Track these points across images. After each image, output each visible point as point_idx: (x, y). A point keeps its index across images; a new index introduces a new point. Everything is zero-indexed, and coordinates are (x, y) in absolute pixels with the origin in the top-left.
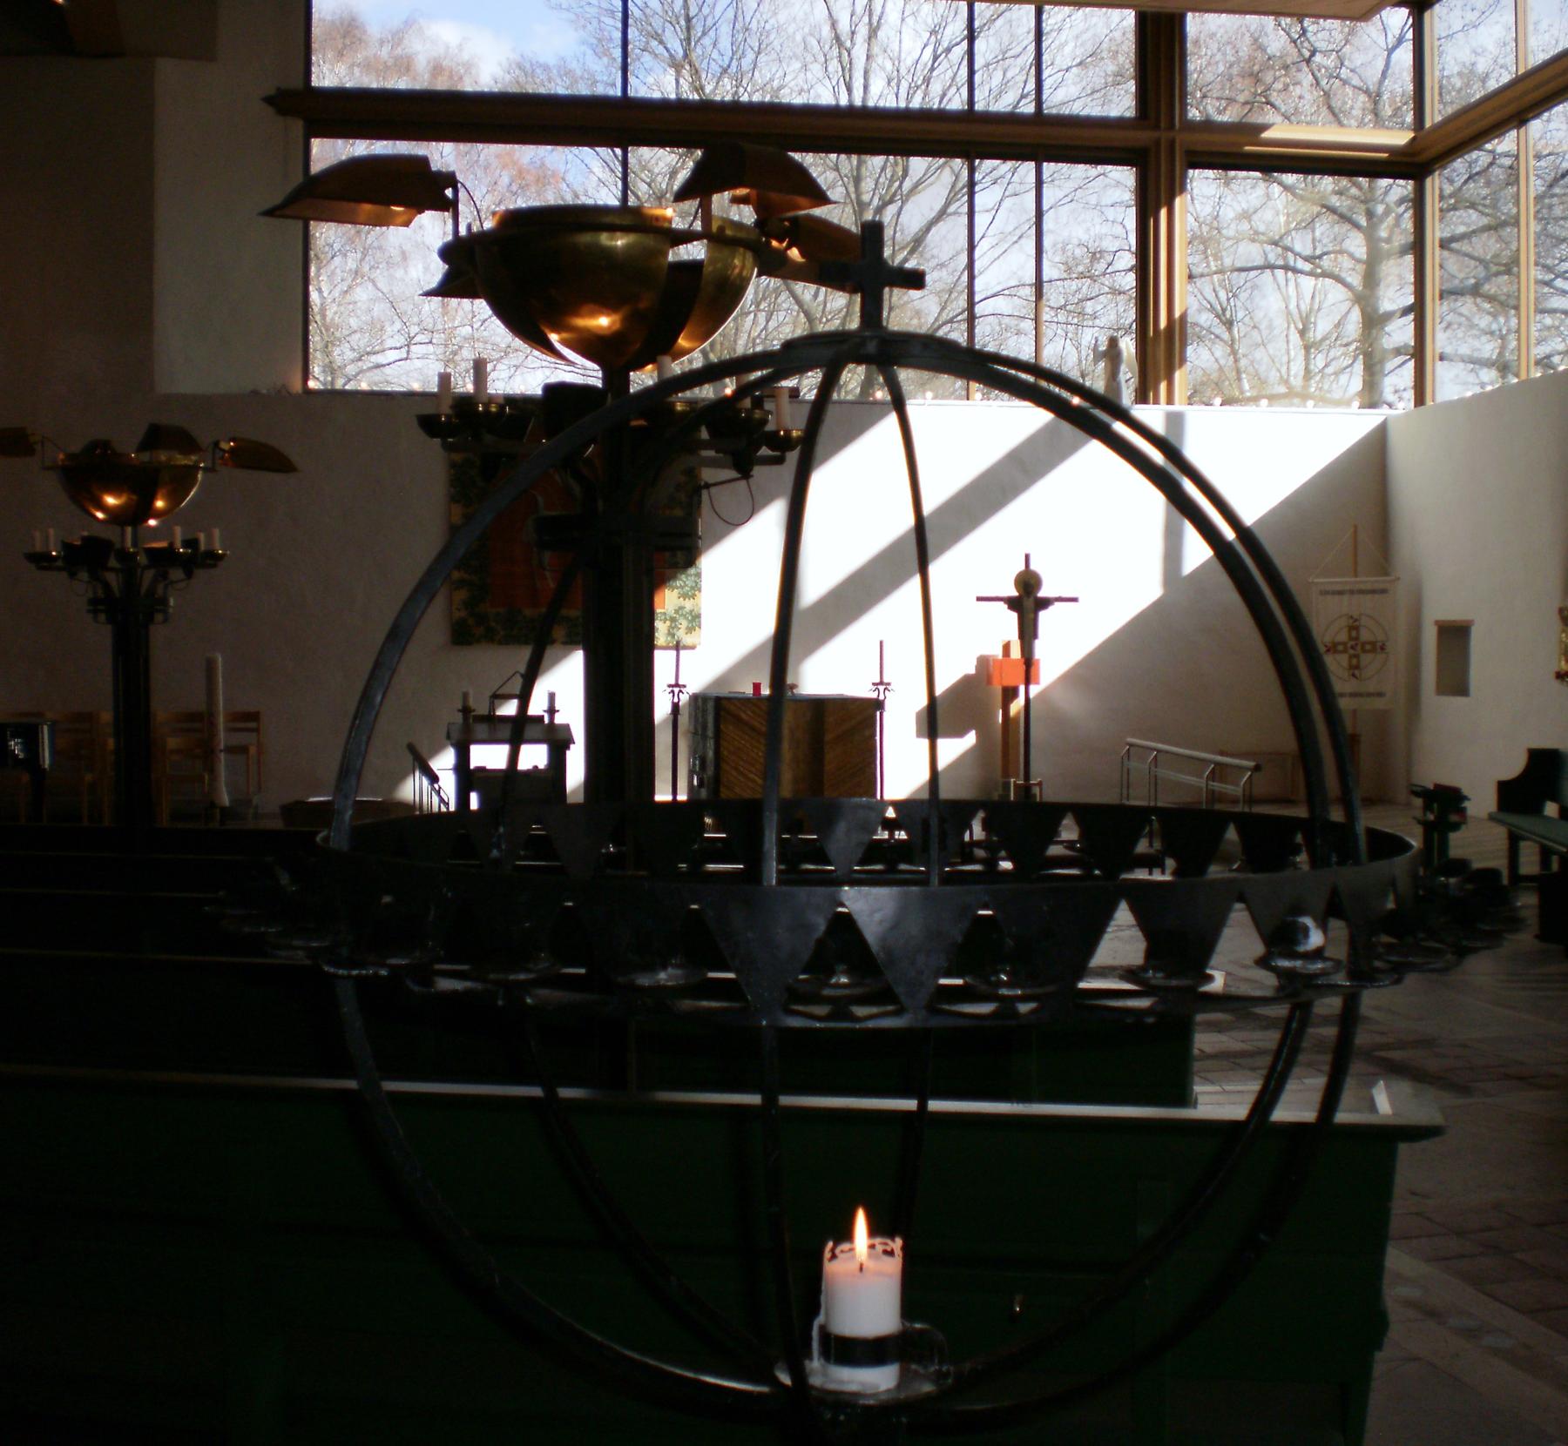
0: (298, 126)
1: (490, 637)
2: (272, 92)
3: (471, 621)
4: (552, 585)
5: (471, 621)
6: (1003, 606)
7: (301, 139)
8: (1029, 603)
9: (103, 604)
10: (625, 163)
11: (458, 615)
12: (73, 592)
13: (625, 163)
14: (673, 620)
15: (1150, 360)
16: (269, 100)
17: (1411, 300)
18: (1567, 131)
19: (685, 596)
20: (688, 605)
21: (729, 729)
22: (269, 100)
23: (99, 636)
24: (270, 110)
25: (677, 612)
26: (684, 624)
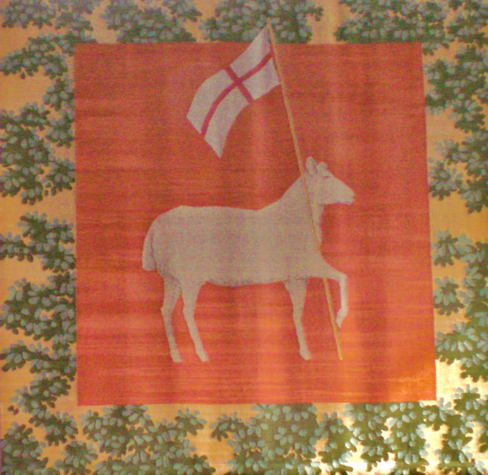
14: (453, 421)
25: (460, 404)
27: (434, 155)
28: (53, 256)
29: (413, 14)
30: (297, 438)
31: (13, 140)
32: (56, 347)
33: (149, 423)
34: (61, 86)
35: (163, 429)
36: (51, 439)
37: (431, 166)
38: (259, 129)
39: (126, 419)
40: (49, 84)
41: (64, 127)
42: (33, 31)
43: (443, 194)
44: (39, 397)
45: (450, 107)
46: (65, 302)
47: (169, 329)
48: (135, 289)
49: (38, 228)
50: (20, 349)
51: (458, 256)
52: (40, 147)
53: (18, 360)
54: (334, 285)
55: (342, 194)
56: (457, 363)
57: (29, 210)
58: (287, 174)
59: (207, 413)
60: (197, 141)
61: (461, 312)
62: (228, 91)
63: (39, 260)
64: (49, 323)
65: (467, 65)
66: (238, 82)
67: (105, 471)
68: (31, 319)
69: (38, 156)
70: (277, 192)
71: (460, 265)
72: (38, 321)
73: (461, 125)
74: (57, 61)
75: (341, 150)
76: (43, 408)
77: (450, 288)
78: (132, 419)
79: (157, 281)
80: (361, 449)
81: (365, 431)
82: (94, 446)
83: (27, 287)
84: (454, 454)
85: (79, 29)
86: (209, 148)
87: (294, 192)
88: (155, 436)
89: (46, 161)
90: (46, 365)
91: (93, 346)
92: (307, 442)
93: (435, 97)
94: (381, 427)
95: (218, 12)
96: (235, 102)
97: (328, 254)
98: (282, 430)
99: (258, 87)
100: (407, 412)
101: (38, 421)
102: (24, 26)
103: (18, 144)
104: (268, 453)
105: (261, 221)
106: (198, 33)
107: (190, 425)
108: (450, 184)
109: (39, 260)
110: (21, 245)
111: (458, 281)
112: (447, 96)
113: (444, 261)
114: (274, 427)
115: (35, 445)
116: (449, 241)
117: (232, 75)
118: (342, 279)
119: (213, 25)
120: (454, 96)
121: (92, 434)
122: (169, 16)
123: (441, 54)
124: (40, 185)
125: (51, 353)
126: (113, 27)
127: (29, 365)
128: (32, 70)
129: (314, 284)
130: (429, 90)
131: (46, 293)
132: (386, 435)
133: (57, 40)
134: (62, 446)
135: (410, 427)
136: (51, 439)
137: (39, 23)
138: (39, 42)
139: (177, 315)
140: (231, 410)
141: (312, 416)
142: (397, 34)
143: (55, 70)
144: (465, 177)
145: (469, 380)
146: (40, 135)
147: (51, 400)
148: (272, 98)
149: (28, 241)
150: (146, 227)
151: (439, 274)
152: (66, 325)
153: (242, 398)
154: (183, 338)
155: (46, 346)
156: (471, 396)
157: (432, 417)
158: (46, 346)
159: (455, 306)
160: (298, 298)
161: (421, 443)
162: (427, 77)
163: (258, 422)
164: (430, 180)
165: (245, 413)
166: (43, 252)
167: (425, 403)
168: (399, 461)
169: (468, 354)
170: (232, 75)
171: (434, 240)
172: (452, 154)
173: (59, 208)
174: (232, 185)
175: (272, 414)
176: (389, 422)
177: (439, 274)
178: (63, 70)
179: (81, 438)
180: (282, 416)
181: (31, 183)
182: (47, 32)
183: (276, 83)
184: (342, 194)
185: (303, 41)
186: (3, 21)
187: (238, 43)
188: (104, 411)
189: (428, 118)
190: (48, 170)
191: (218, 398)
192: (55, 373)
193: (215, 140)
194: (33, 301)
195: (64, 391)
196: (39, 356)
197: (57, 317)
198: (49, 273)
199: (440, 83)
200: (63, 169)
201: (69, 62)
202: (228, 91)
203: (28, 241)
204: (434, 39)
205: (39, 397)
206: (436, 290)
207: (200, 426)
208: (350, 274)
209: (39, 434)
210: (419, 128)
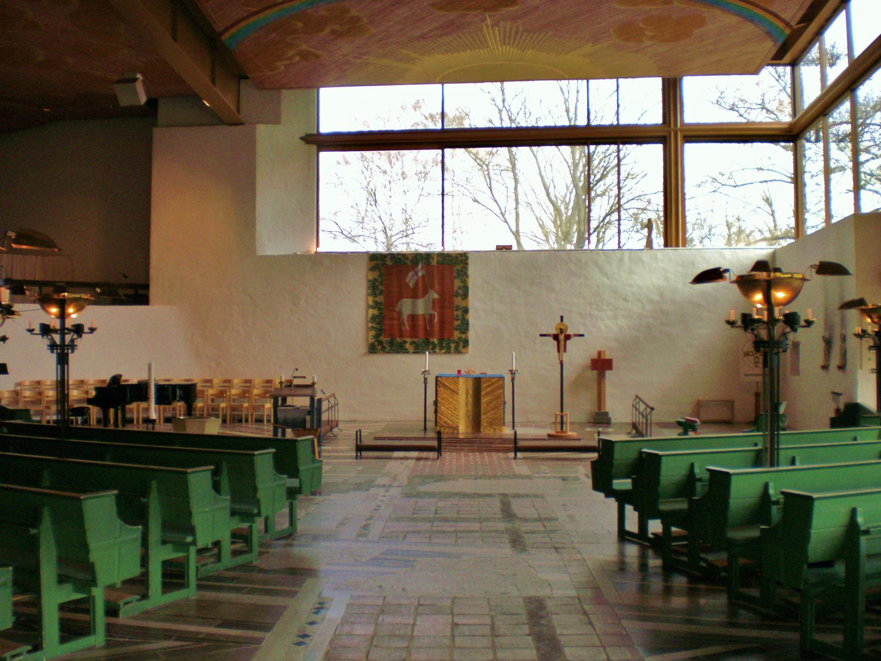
0: (315, 147)
1: (384, 350)
2: (304, 135)
3: (376, 344)
4: (408, 328)
5: (376, 344)
6: (551, 339)
7: (315, 152)
8: (562, 337)
9: (53, 346)
10: (618, 119)
11: (370, 341)
12: (43, 343)
13: (618, 119)
14: (457, 343)
15: (800, 205)
16: (302, 138)
17: (832, 176)
18: (880, 84)
19: (462, 333)
20: (463, 336)
21: (441, 390)
22: (302, 138)
23: (53, 358)
24: (302, 142)
26: (461, 344)
27: (455, 288)
28: (379, 309)
38: (420, 285)
47: (647, 614)
48: (395, 315)
55: (436, 296)
58: (425, 292)
59: (409, 340)
60: (407, 285)
66: (416, 273)
67: (378, 486)
75: (437, 287)
87: (427, 296)
91: (467, 42)
96: (415, 277)
99: (420, 274)
106: (409, 263)
107: (405, 342)
112: (459, 276)
118: (436, 314)
130: (455, 275)
140: (413, 340)
148: (423, 277)
151: (455, 313)
165: (416, 340)
174: (415, 296)
175: (421, 341)
177: (455, 313)
184: (436, 296)
187: (417, 264)
188: (388, 339)
191: (412, 337)
193: (411, 285)
210: (453, 283)
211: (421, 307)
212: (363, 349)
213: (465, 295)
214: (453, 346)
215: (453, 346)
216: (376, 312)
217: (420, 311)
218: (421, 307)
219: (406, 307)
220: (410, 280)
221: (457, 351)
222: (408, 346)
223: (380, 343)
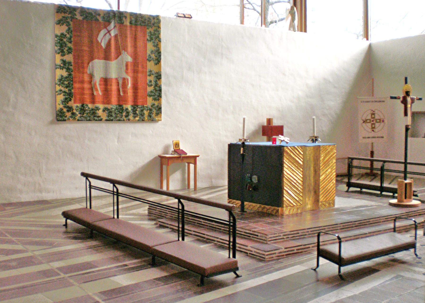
14: (151, 110)
25: (152, 106)
27: (149, 52)
28: (68, 69)
29: (145, 20)
30: (120, 113)
31: (59, 41)
32: (69, 90)
33: (89, 108)
34: (69, 28)
35: (92, 109)
36: (68, 111)
37: (148, 54)
39: (84, 107)
40: (67, 28)
41: (70, 39)
42: (63, 15)
43: (150, 61)
44: (65, 102)
45: (152, 42)
46: (70, 80)
49: (64, 62)
50: (61, 90)
51: (152, 74)
52: (65, 43)
53: (60, 93)
54: (128, 80)
56: (151, 97)
57: (62, 58)
58: (118, 54)
60: (99, 44)
61: (153, 86)
62: (119, 8)
63: (65, 70)
64: (67, 84)
65: (155, 33)
66: (109, 32)
68: (63, 83)
69: (64, 45)
70: (117, 57)
71: (153, 76)
72: (64, 84)
73: (154, 46)
74: (68, 22)
76: (66, 104)
77: (151, 81)
78: (86, 107)
79: (91, 76)
80: (132, 115)
81: (133, 111)
82: (77, 113)
83: (62, 76)
84: (150, 116)
85: (74, 15)
86: (102, 46)
88: (90, 111)
89: (66, 47)
90: (66, 94)
92: (121, 113)
93: (149, 39)
94: (137, 110)
95: (105, 15)
96: (107, 37)
97: (127, 73)
98: (116, 110)
100: (141, 107)
101: (65, 107)
102: (61, 13)
103: (59, 42)
104: (114, 115)
105: (113, 64)
107: (98, 109)
108: (151, 59)
109: (65, 70)
110: (60, 66)
111: (152, 80)
112: (151, 39)
113: (150, 75)
114: (115, 109)
115: (64, 112)
116: (151, 71)
117: (107, 30)
118: (129, 79)
119: (104, 18)
120: (153, 39)
121: (77, 110)
122: (94, 14)
123: (150, 29)
124: (64, 52)
125: (67, 91)
126: (81, 16)
127: (62, 94)
128: (63, 24)
129: (124, 79)
130: (148, 38)
131: (66, 78)
132: (137, 112)
133: (68, 17)
134: (70, 113)
135: (142, 111)
136: (68, 111)
137: (65, 13)
138: (64, 17)
139: (95, 84)
140: (106, 106)
141: (123, 108)
142: (142, 24)
143: (68, 25)
144: (154, 57)
145: (154, 101)
146: (65, 40)
147: (68, 103)
149: (62, 65)
150: (88, 64)
152: (70, 85)
153: (109, 104)
154: (97, 90)
155: (67, 90)
156: (154, 105)
157: (146, 109)
158: (67, 90)
159: (151, 85)
160: (121, 82)
161: (144, 114)
162: (148, 34)
163: (112, 108)
164: (147, 58)
166: (65, 68)
167: (145, 106)
168: (140, 118)
169: (154, 96)
170: (107, 30)
171: (148, 71)
172: (152, 52)
173: (69, 58)
176: (138, 109)
177: (149, 78)
178: (70, 25)
179: (74, 111)
180: (117, 107)
181: (62, 51)
182: (66, 15)
183: (116, 33)
185: (123, 23)
186: (366, 39)
187: (109, 23)
189: (147, 44)
190: (66, 48)
192: (68, 96)
193: (103, 45)
194: (63, 79)
195: (70, 100)
196: (65, 92)
197: (69, 83)
198: (67, 73)
199: (150, 36)
200: (70, 49)
201: (71, 23)
202: (119, 8)
203: (62, 65)
204: (149, 26)
205: (65, 102)
206: (148, 82)
207: (100, 109)
208: (130, 77)
209: (65, 110)
211: (115, 69)
212: (50, 116)
213: (158, 61)
214: (146, 113)
215: (146, 113)
216: (65, 74)
217: (113, 75)
218: (115, 69)
219: (98, 68)
220: (102, 39)
221: (151, 120)
222: (100, 113)
223: (70, 109)
